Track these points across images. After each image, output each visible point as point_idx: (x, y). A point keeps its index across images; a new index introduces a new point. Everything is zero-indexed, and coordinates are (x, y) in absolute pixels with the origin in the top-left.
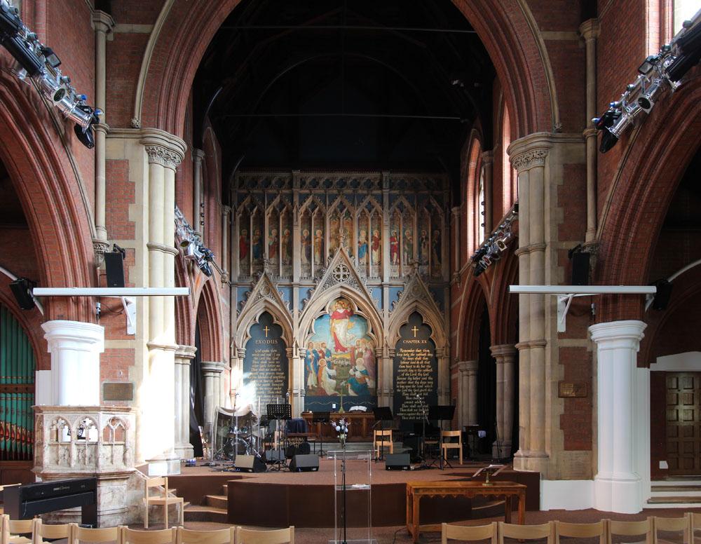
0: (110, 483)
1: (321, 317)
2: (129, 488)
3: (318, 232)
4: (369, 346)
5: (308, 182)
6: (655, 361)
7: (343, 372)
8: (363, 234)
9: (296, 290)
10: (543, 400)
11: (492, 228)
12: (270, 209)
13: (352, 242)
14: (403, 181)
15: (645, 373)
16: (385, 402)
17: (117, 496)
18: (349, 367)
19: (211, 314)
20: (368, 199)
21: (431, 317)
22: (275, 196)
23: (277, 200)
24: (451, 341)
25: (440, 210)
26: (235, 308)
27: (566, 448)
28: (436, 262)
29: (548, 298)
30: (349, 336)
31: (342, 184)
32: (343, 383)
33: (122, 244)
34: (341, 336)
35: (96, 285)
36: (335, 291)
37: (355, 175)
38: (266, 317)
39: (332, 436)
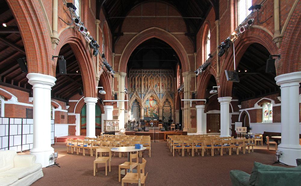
1: (147, 100)
3: (147, 82)
4: (157, 106)
5: (144, 72)
6: (208, 112)
7: (152, 112)
8: (156, 82)
9: (142, 95)
10: (188, 119)
11: (181, 84)
12: (137, 78)
13: (154, 84)
14: (164, 71)
15: (205, 114)
16: (161, 119)
19: (91, 77)
20: (157, 75)
21: (170, 100)
22: (138, 75)
23: (138, 75)
24: (174, 105)
25: (172, 77)
26: (130, 98)
27: (192, 127)
28: (171, 88)
29: (189, 102)
30: (153, 104)
31: (152, 72)
32: (152, 114)
33: (117, 92)
34: (151, 104)
35: (112, 100)
36: (150, 95)
37: (154, 70)
38: (136, 100)
39: (150, 125)
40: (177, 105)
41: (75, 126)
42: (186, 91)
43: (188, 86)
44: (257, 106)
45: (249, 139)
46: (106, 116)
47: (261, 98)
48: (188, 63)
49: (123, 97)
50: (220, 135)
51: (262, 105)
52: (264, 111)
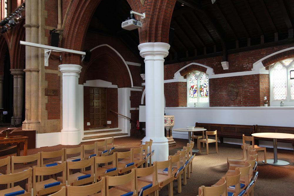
10: (38, 97)
15: (81, 87)
27: (49, 119)
44: (258, 68)
45: (166, 139)
47: (187, 62)
50: (169, 142)
51: (186, 75)
52: (189, 87)
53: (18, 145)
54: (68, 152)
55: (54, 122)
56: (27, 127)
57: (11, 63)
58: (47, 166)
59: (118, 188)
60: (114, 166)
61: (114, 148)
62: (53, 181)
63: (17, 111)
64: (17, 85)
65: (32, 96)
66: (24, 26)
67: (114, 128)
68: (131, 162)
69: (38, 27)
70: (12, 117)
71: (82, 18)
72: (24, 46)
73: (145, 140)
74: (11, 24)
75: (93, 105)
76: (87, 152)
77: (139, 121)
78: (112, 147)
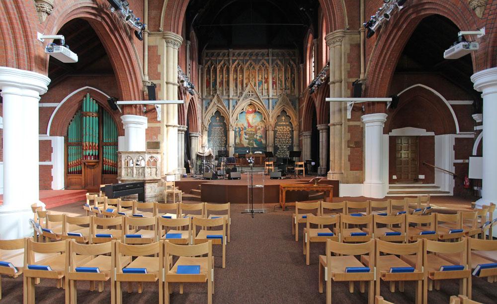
0: (150, 184)
2: (158, 186)
8: (260, 76)
10: (341, 149)
12: (219, 66)
13: (255, 80)
15: (387, 137)
16: (270, 149)
17: (153, 189)
18: (254, 134)
19: (130, 74)
20: (263, 61)
21: (290, 112)
23: (223, 62)
25: (294, 65)
27: (351, 170)
30: (254, 121)
31: (251, 55)
33: (155, 82)
34: (250, 121)
36: (248, 101)
37: (257, 51)
38: (218, 112)
39: (246, 164)
40: (305, 123)
41: (51, 167)
42: (337, 78)
43: (341, 66)
46: (127, 143)
48: (341, 9)
49: (174, 90)
53: (325, 192)
54: (373, 204)
55: (357, 173)
56: (331, 176)
57: (318, 120)
58: (352, 215)
59: (439, 256)
60: (432, 229)
61: (430, 207)
62: (358, 231)
63: (322, 162)
64: (323, 139)
65: (336, 148)
66: (329, 83)
67: (428, 183)
68: (458, 228)
69: (341, 82)
70: (319, 168)
71: (388, 61)
72: (329, 102)
73: (479, 203)
74: (318, 85)
75: (400, 156)
76: (395, 208)
77: (469, 178)
78: (428, 206)
